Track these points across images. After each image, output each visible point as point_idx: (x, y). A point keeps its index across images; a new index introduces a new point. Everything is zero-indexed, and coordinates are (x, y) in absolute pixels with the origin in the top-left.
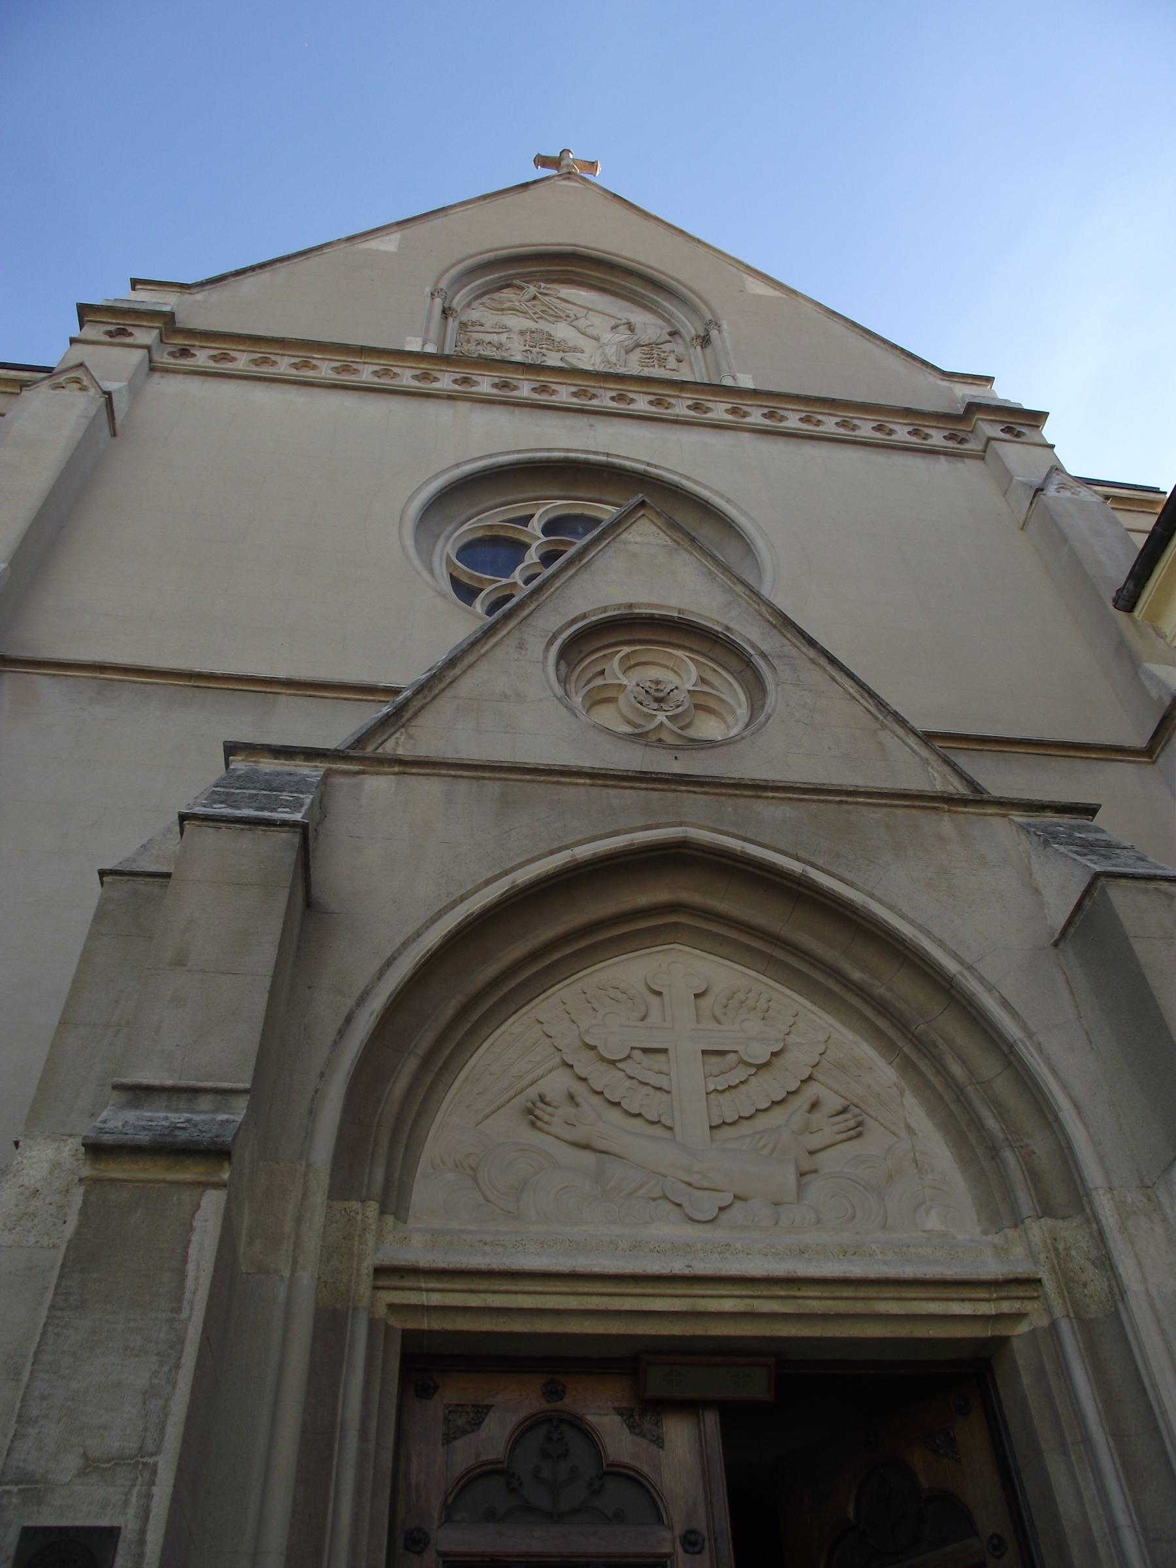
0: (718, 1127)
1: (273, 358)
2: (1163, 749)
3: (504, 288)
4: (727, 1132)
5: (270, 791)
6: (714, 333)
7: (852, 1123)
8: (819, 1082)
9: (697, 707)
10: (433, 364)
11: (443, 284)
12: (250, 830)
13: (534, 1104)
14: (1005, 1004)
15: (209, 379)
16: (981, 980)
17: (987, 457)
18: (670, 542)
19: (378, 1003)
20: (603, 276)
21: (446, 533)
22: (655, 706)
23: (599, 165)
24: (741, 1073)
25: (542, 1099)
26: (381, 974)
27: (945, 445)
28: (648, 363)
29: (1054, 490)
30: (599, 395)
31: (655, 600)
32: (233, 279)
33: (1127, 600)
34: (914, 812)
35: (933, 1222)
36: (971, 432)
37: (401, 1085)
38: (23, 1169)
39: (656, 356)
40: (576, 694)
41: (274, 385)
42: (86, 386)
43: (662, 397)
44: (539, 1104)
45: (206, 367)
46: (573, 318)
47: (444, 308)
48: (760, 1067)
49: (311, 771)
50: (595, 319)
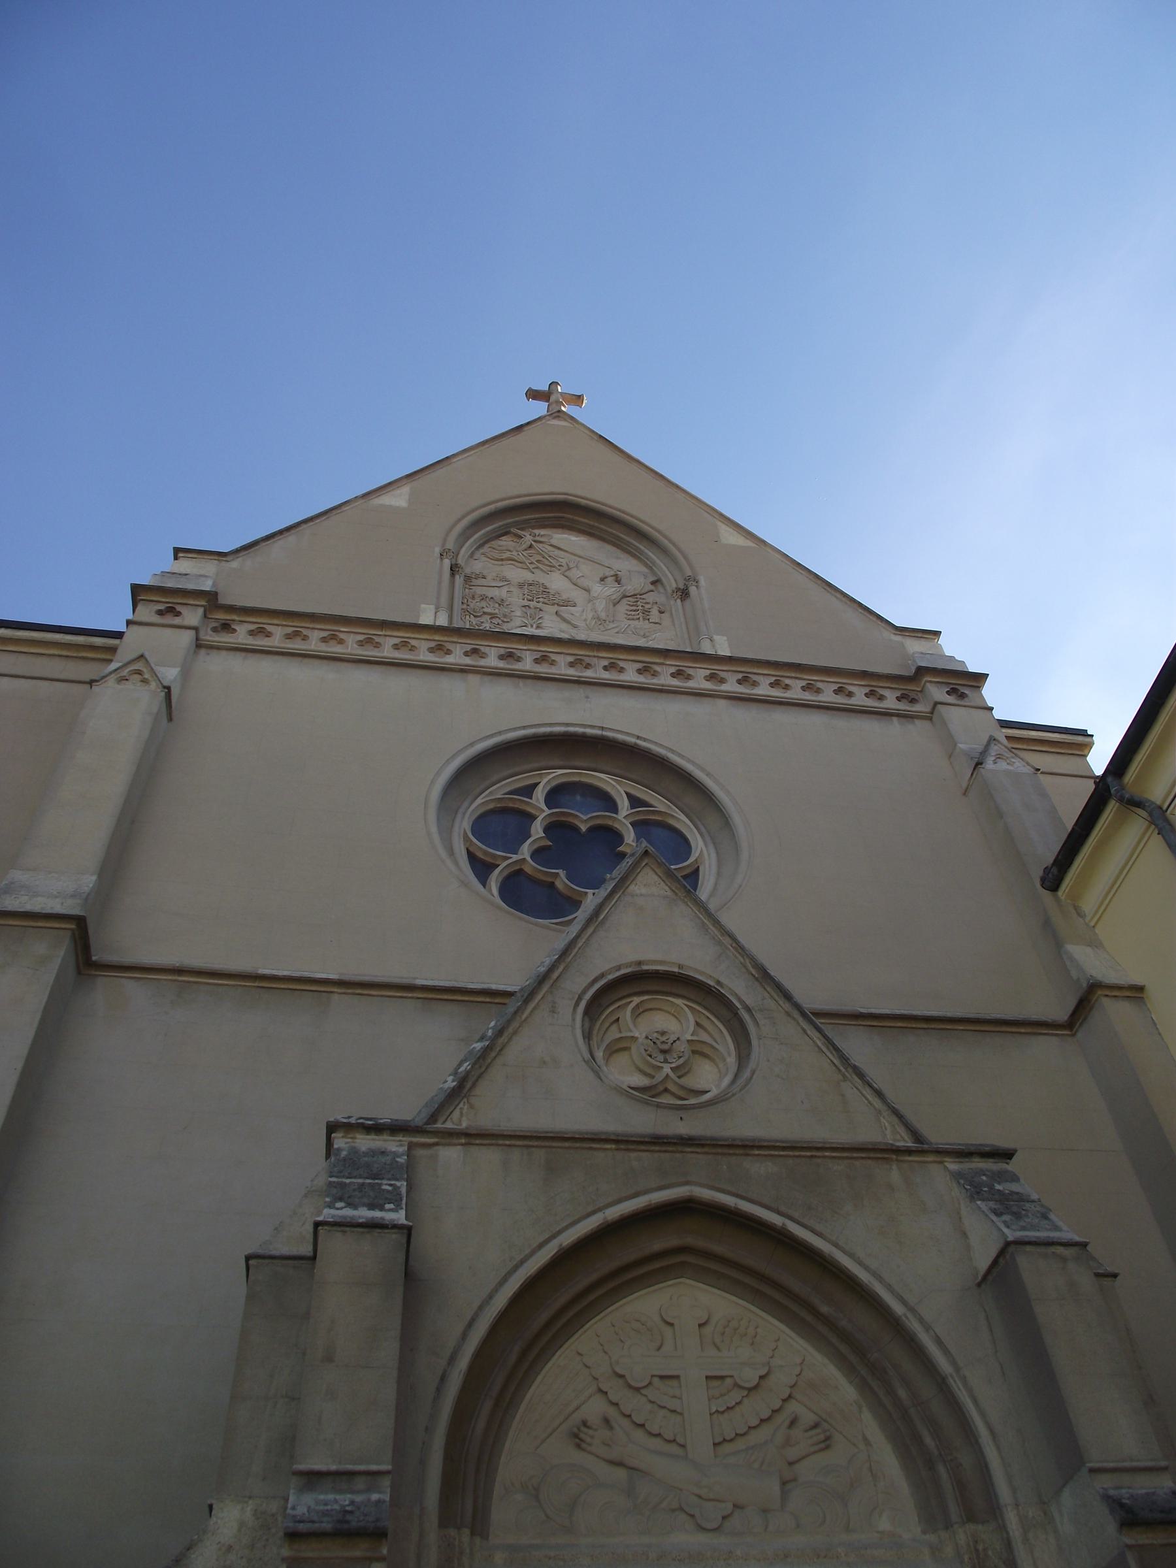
0: (719, 1444)
1: (305, 632)
2: (1081, 1024)
3: (504, 536)
4: (727, 1448)
5: (372, 1179)
6: (693, 590)
7: (822, 1437)
8: (796, 1400)
9: (694, 1052)
10: (446, 635)
11: (450, 545)
12: (368, 1232)
13: (579, 1429)
14: (939, 1342)
15: (250, 655)
16: (921, 1320)
17: (935, 717)
18: (669, 893)
19: (463, 1363)
20: (592, 523)
21: (461, 810)
22: (661, 1057)
23: (585, 398)
24: (735, 1396)
25: (585, 1423)
26: (464, 1336)
27: (898, 707)
28: (634, 615)
29: (991, 762)
30: (593, 664)
31: (659, 957)
32: (264, 544)
33: (1054, 878)
34: (870, 1162)
35: (884, 1524)
36: (921, 691)
37: (481, 1425)
38: (218, 1529)
39: (640, 608)
40: (598, 1049)
41: (306, 660)
42: (147, 679)
43: (649, 665)
44: (583, 1429)
45: (246, 645)
46: (565, 567)
47: (451, 565)
48: (750, 1390)
49: (395, 1145)
50: (585, 568)
